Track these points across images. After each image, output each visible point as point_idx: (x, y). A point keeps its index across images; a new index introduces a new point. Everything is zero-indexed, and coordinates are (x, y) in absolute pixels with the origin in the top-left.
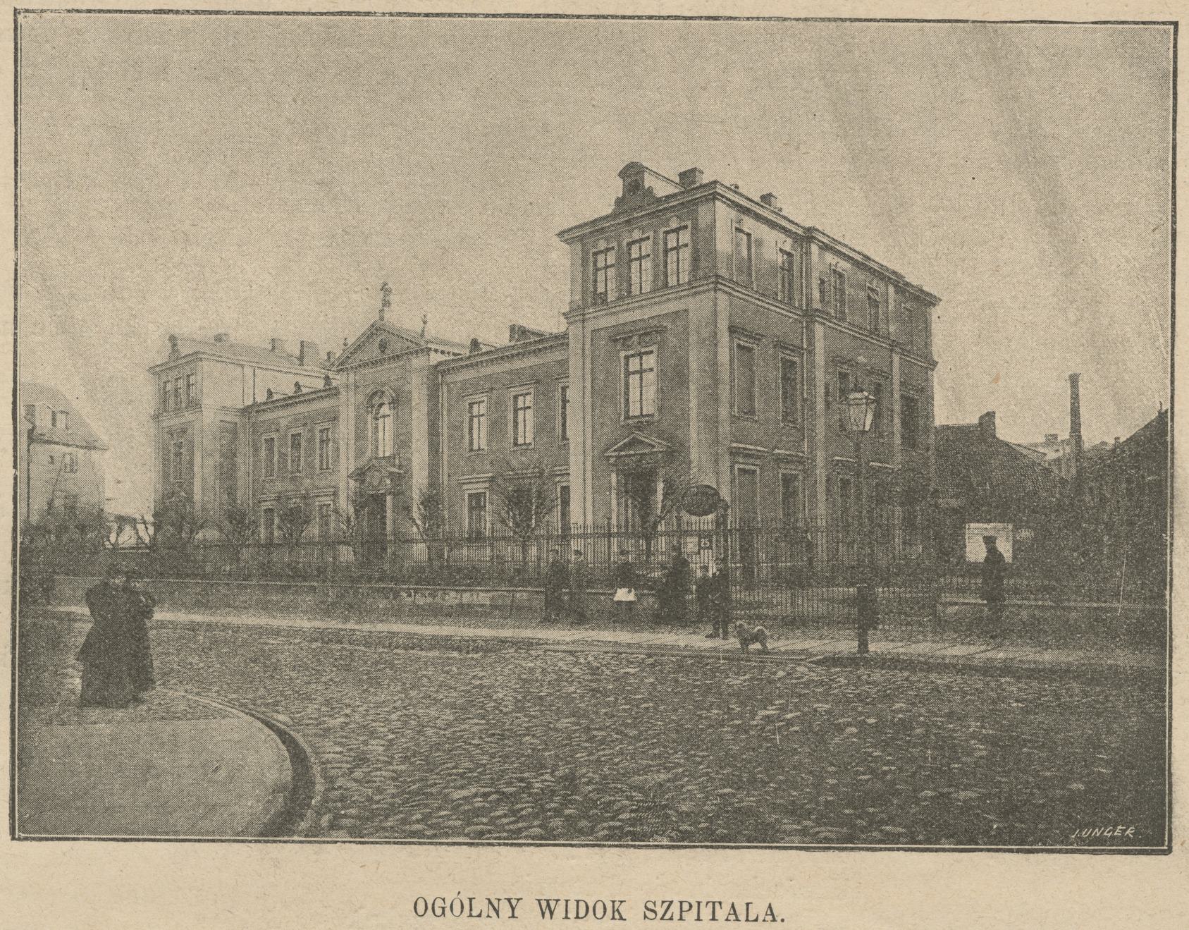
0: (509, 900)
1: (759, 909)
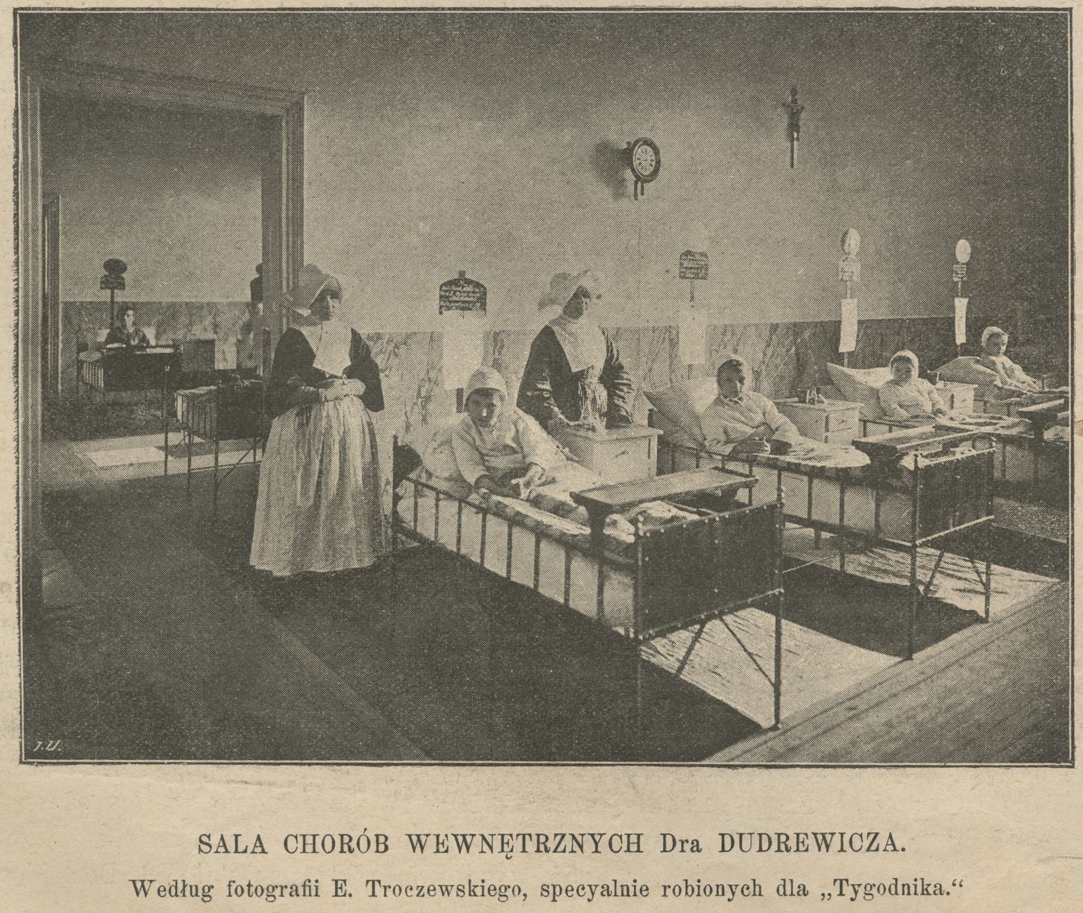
0: (592, 835)
1: (247, 841)
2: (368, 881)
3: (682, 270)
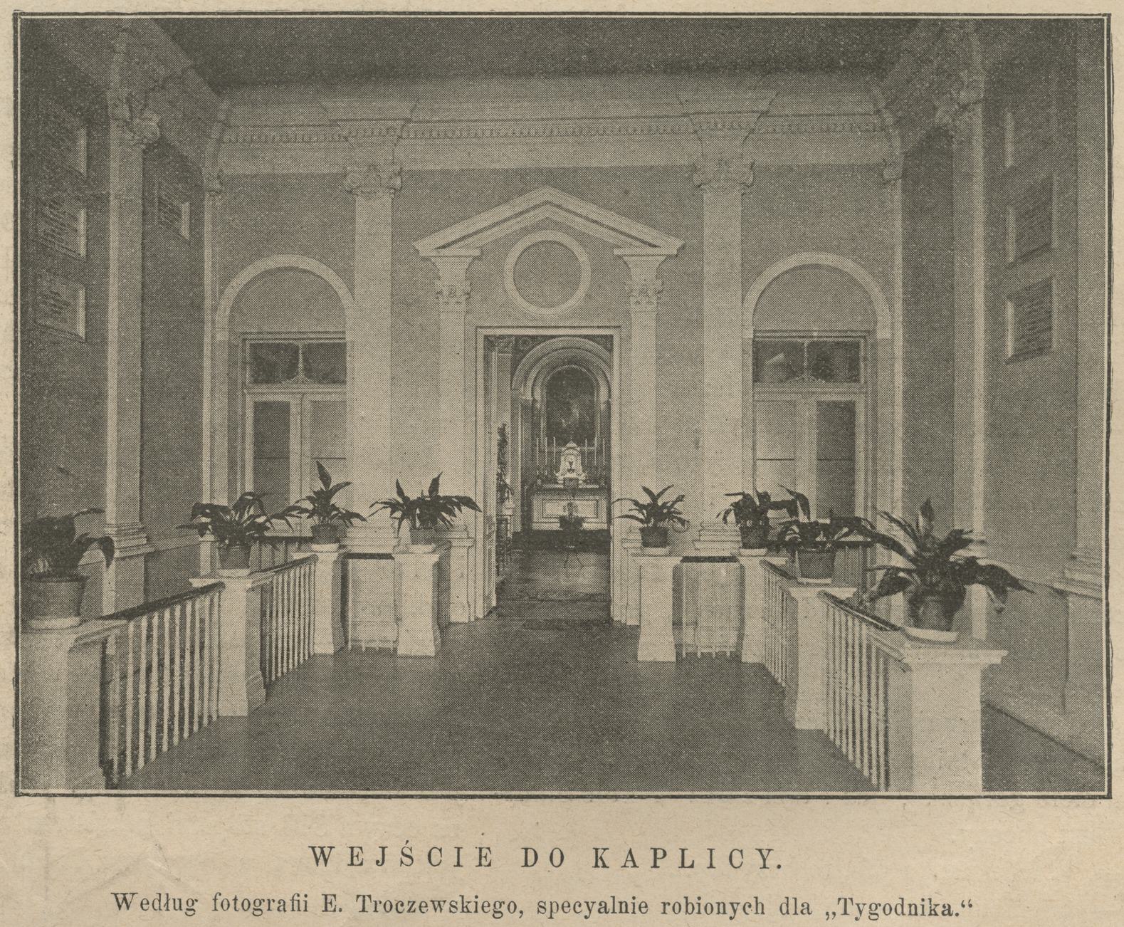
2: (692, 866)
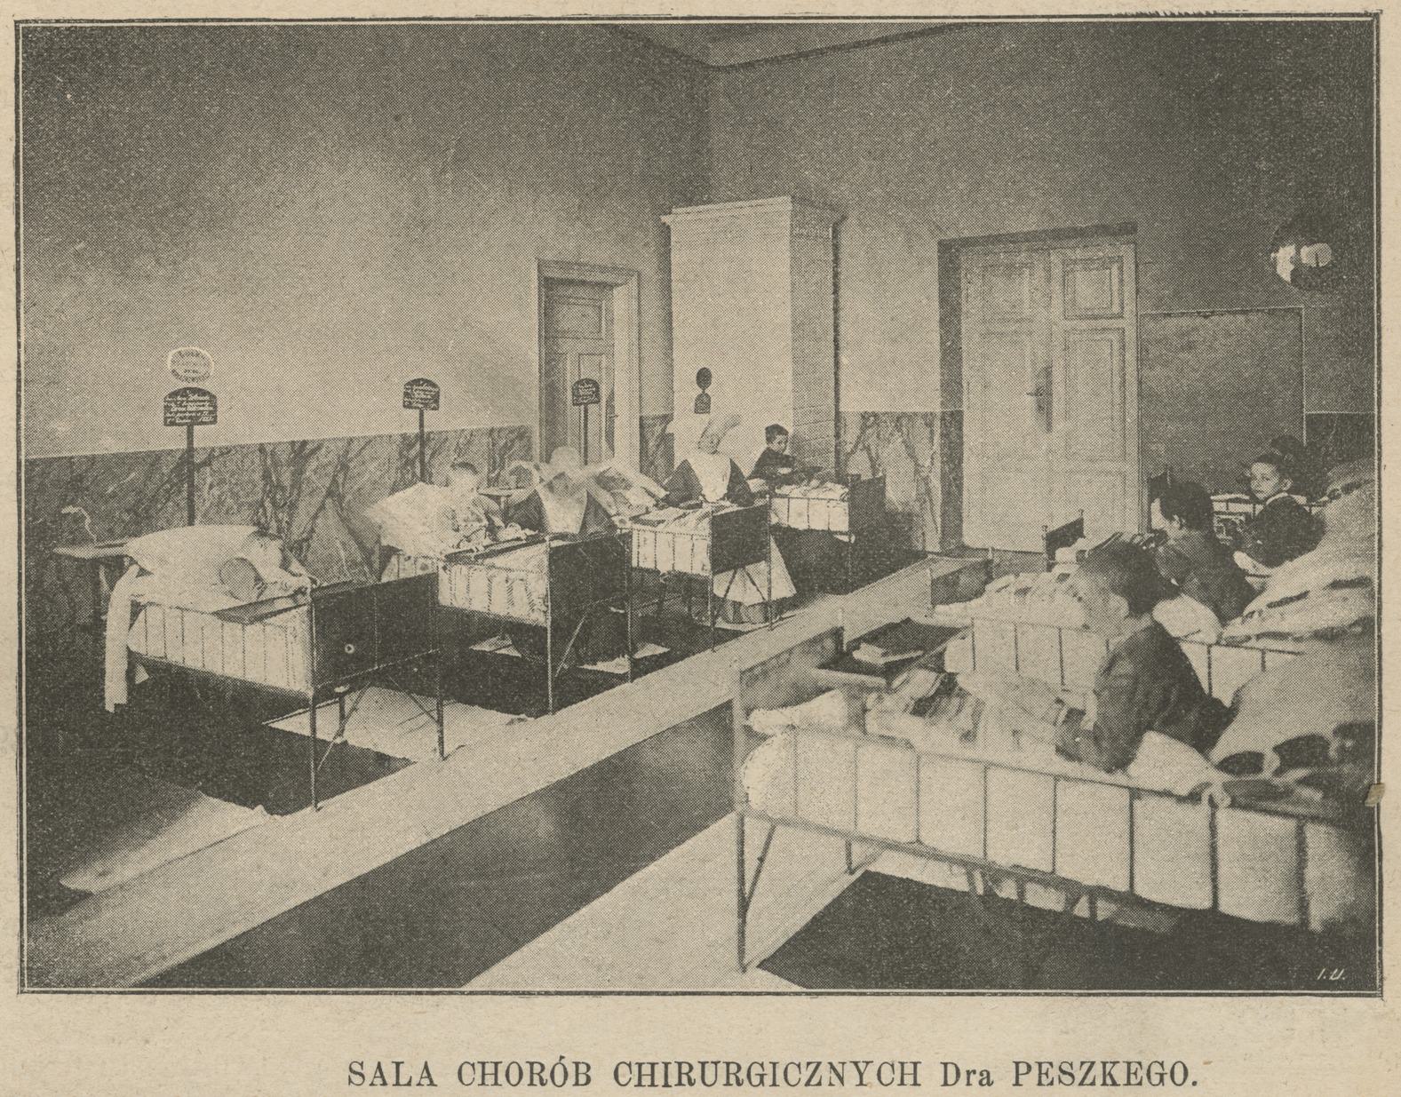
0: (856, 1064)
1: (411, 1071)
3: (168, 415)
